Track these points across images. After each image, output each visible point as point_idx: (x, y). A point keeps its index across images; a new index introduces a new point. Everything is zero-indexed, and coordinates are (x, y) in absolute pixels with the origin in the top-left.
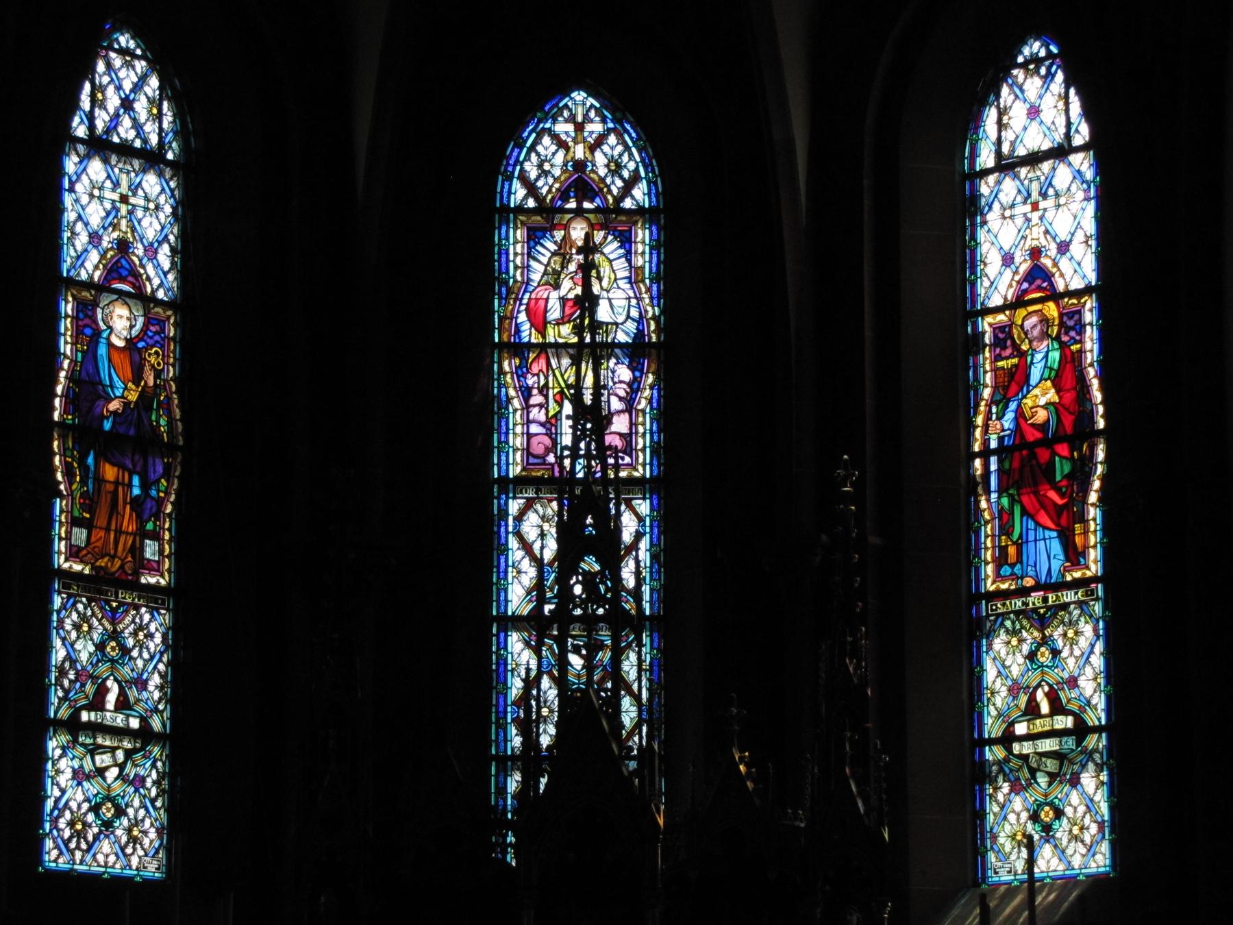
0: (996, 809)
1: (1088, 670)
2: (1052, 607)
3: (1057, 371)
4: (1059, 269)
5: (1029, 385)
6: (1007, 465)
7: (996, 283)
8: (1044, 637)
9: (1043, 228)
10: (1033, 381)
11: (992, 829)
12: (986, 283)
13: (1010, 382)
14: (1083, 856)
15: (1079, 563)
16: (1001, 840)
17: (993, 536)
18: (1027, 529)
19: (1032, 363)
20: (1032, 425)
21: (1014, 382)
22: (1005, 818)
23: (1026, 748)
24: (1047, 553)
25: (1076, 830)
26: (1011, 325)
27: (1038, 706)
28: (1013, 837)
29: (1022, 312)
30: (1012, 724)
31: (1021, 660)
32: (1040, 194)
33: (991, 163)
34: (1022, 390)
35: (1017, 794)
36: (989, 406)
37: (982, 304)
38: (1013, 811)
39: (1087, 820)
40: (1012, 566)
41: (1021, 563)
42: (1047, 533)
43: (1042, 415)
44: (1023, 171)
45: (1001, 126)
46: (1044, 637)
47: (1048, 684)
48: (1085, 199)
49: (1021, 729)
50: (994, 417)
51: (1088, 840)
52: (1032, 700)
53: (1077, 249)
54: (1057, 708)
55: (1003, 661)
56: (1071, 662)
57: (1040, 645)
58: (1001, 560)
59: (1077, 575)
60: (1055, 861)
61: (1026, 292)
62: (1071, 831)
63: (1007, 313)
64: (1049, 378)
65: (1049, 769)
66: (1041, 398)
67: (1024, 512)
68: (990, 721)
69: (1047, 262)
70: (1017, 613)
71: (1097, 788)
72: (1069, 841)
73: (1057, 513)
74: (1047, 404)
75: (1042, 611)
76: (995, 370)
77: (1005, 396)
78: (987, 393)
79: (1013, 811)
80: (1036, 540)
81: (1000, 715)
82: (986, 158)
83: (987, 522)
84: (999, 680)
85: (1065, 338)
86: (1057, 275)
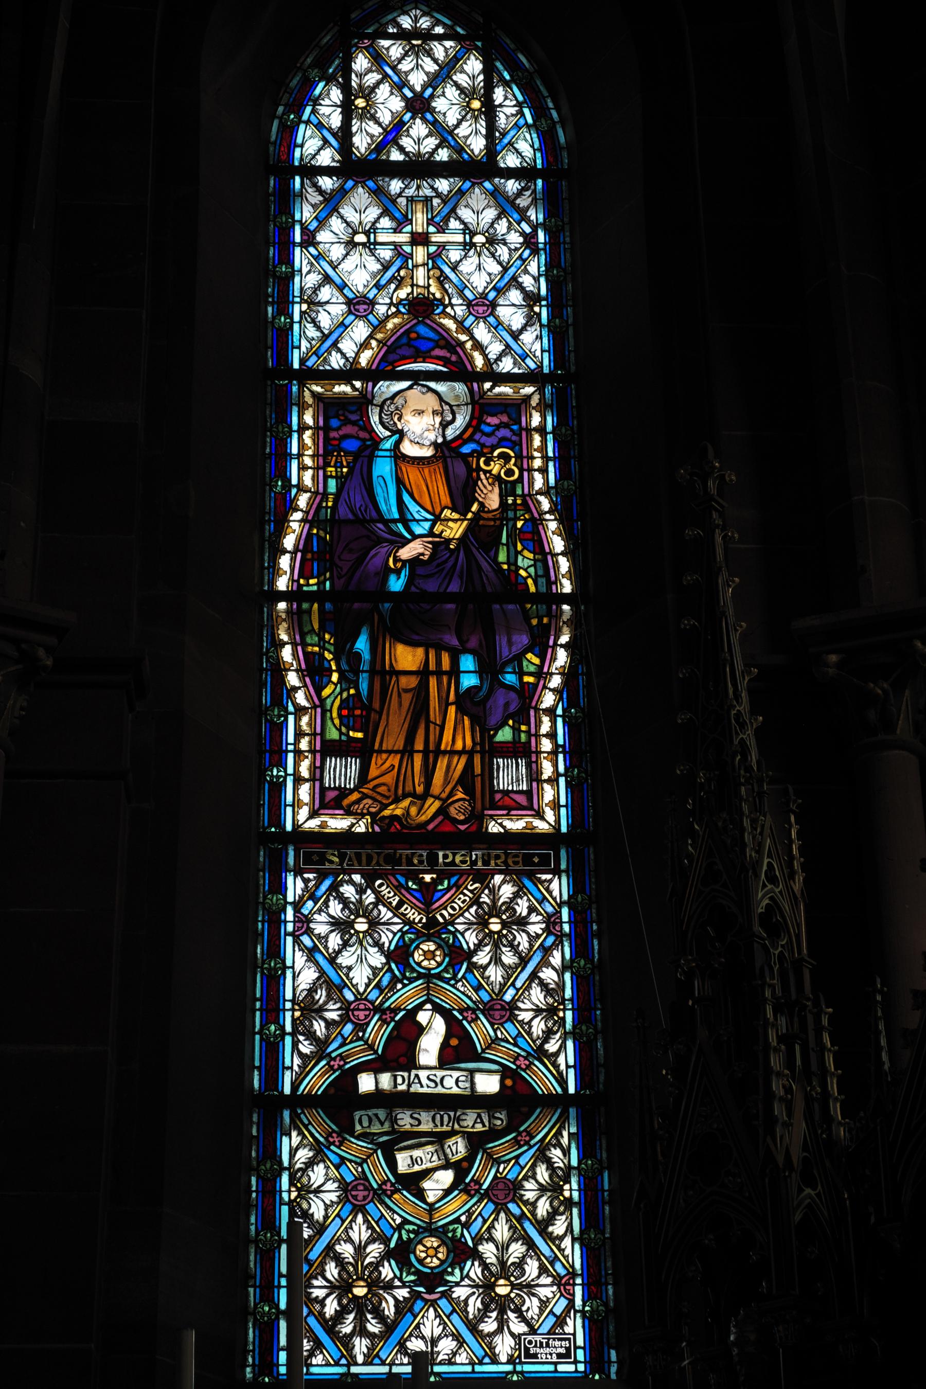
4: (472, 337)
32: (430, 222)
44: (395, 186)
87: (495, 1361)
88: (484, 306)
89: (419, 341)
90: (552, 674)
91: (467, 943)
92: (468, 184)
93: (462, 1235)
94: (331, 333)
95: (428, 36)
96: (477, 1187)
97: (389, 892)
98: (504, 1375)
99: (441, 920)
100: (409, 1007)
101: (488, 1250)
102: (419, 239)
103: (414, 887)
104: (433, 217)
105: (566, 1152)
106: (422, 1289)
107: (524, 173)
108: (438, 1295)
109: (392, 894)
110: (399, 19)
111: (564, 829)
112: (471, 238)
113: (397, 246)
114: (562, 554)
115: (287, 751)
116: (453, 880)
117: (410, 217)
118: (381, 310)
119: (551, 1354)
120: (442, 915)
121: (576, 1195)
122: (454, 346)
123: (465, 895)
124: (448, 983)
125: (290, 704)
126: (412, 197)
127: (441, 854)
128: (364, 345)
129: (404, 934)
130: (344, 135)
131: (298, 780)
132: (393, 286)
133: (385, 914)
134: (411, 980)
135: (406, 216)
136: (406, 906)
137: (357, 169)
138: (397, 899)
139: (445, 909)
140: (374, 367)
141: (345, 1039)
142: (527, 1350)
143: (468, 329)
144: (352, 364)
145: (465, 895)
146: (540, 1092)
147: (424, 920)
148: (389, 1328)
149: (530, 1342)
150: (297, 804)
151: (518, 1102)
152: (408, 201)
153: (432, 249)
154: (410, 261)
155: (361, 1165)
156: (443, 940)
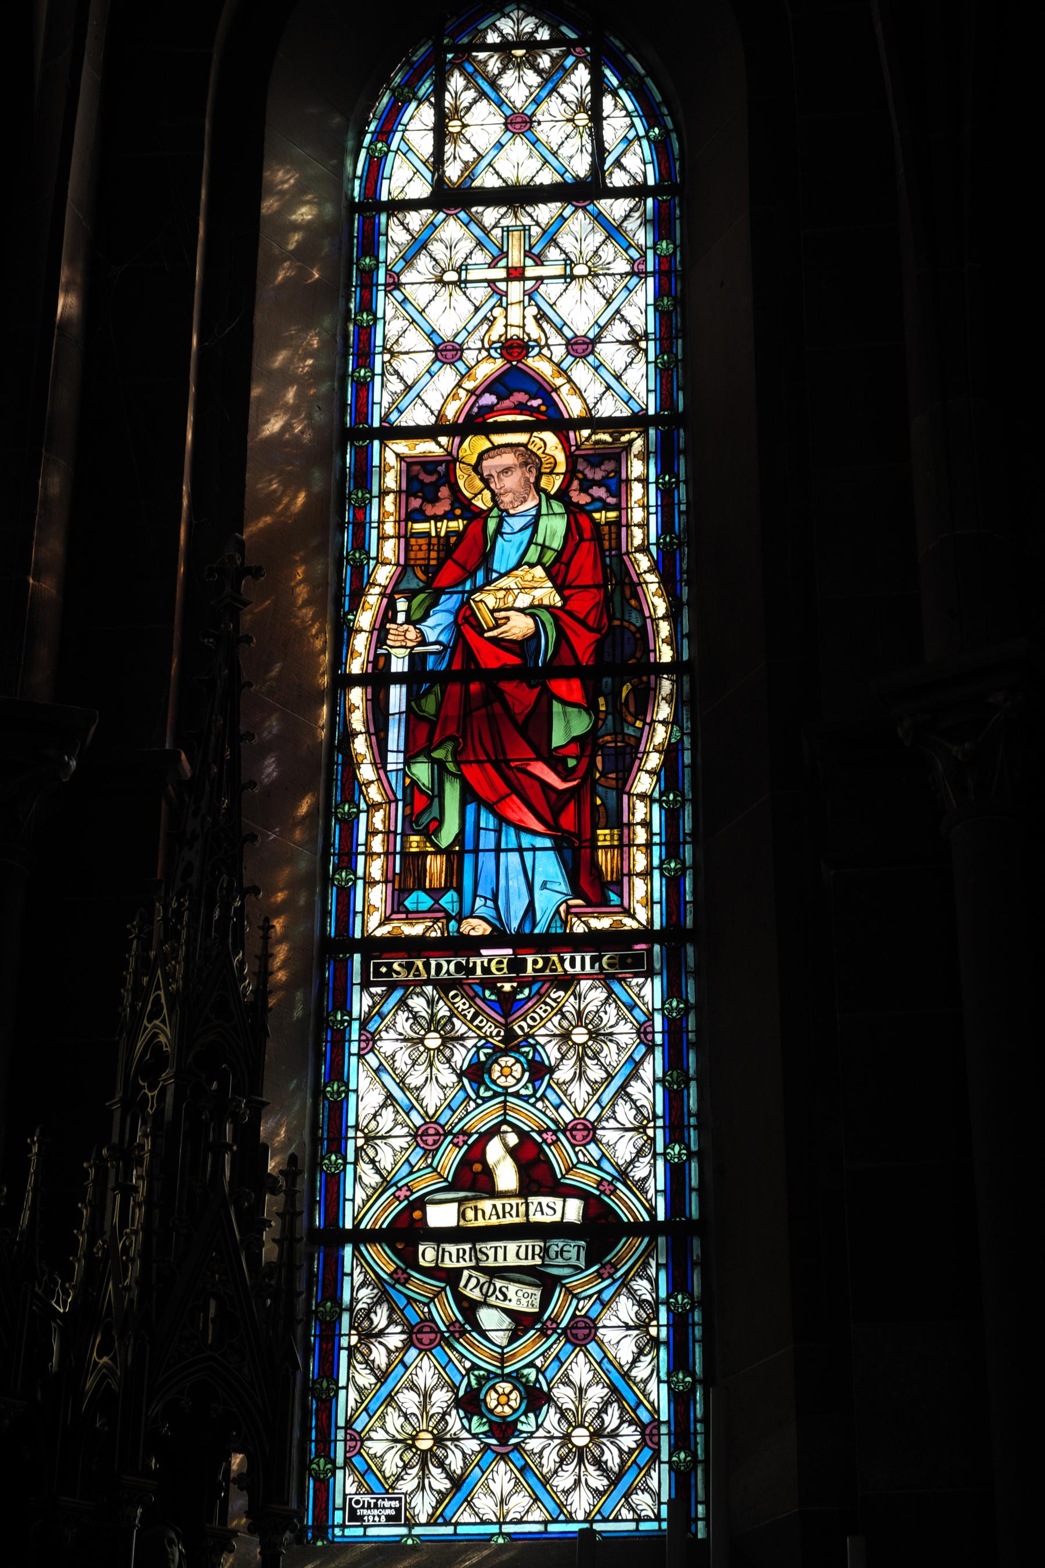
0: (365, 1378)
1: (625, 1113)
2: (534, 980)
3: (560, 553)
4: (570, 380)
5: (489, 570)
6: (430, 705)
7: (416, 388)
8: (510, 1036)
9: (532, 311)
10: (500, 564)
11: (349, 1423)
12: (395, 385)
13: (441, 563)
14: (597, 1493)
15: (605, 902)
16: (376, 1447)
17: (388, 833)
18: (478, 828)
19: (499, 531)
20: (494, 640)
21: (457, 561)
22: (390, 1399)
23: (454, 1257)
24: (531, 881)
25: (581, 1438)
26: (451, 460)
27: (488, 1173)
28: (409, 1443)
29: (474, 446)
30: (421, 1204)
31: (448, 1078)
32: (528, 254)
33: (420, 190)
34: (473, 575)
35: (425, 1350)
36: (389, 598)
37: (384, 419)
38: (413, 1387)
39: (612, 1418)
40: (437, 894)
41: (459, 890)
42: (526, 840)
43: (519, 626)
44: (490, 215)
45: (440, 134)
46: (510, 1036)
47: (516, 1129)
48: (632, 274)
49: (441, 1216)
50: (401, 618)
51: (612, 1458)
52: (476, 1154)
53: (613, 354)
54: (537, 1176)
55: (399, 1083)
56: (579, 1092)
57: (498, 1053)
58: (408, 876)
59: (603, 923)
60: (519, 1503)
61: (490, 409)
62: (567, 1437)
63: (443, 440)
64: (539, 562)
65: (512, 1305)
66: (518, 599)
67: (467, 796)
68: (361, 1195)
69: (536, 363)
70: (444, 986)
71: (641, 1352)
72: (562, 1461)
73: (550, 809)
74: (532, 606)
75: (507, 987)
76: (405, 537)
77: (428, 584)
78: (383, 575)
79: (413, 1387)
80: (498, 850)
81: (386, 1183)
82: (405, 179)
83: (373, 807)
84: (388, 1114)
85: (579, 498)
86: (565, 390)
87: (570, 1520)
88: (582, 347)
89: (517, 390)
90: (649, 752)
91: (548, 1058)
92: (569, 209)
93: (537, 1380)
94: (415, 383)
95: (533, 46)
96: (554, 1326)
97: (464, 1004)
98: (398, 1539)
99: (520, 1033)
100: (482, 1130)
101: (564, 1395)
102: (516, 274)
103: (493, 997)
104: (531, 247)
105: (655, 1283)
106: (493, 1441)
107: (637, 191)
108: (511, 1448)
109: (467, 1005)
110: (498, 23)
111: (657, 926)
112: (572, 269)
113: (491, 283)
114: (663, 618)
115: (357, 854)
116: (535, 988)
117: (505, 250)
118: (470, 356)
119: (379, 1516)
120: (521, 1027)
121: (664, 1333)
122: (544, 391)
123: (547, 1004)
124: (527, 1102)
125: (362, 800)
126: (508, 227)
127: (530, 959)
128: (453, 395)
129: (479, 1049)
130: (438, 160)
131: (369, 883)
132: (485, 327)
133: (460, 1027)
134: (485, 1100)
135: (501, 250)
136: (480, 1018)
137: (451, 198)
138: (472, 1010)
139: (525, 1020)
140: (460, 421)
141: (412, 1167)
142: (353, 1511)
143: (565, 372)
144: (437, 417)
145: (547, 1004)
146: (625, 1220)
147: (502, 1033)
148: (457, 1482)
149: (357, 1502)
150: (368, 908)
151: (600, 1231)
152: (503, 231)
153: (529, 284)
154: (504, 299)
155: (427, 1305)
156: (522, 1054)
